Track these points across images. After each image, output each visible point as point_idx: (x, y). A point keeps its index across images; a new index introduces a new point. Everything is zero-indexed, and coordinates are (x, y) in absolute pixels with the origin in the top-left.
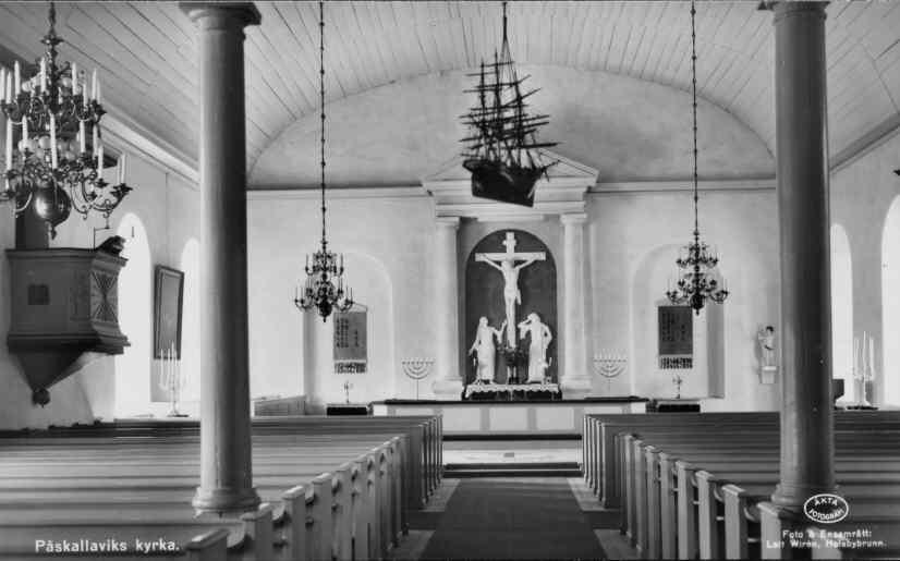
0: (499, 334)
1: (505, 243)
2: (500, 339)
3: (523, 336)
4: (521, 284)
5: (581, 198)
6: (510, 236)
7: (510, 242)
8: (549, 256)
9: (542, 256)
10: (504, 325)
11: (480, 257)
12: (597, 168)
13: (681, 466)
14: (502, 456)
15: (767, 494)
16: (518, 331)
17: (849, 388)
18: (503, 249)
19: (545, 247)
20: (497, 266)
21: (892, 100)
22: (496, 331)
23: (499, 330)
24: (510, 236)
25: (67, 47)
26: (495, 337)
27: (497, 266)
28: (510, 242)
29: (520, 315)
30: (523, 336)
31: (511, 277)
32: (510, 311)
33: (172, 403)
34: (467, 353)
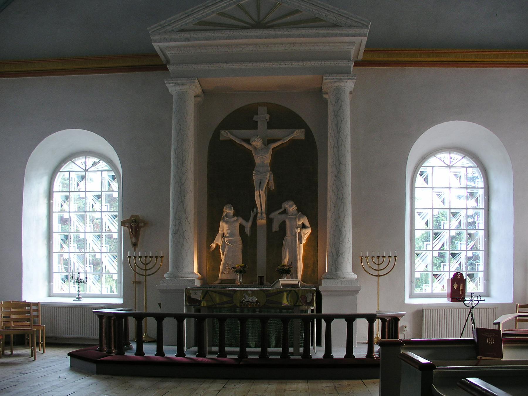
0: (248, 225)
1: (255, 118)
2: (248, 231)
3: (275, 227)
5: (296, 212)
7: (263, 117)
8: (308, 133)
9: (299, 134)
10: (252, 215)
11: (226, 135)
12: (236, 355)
13: (458, 383)
16: (270, 221)
18: (254, 126)
19: (215, 132)
20: (245, 145)
22: (244, 223)
26: (242, 228)
27: (245, 145)
28: (263, 117)
29: (274, 202)
30: (275, 227)
31: (263, 159)
32: (261, 199)
33: (86, 213)
34: (209, 247)
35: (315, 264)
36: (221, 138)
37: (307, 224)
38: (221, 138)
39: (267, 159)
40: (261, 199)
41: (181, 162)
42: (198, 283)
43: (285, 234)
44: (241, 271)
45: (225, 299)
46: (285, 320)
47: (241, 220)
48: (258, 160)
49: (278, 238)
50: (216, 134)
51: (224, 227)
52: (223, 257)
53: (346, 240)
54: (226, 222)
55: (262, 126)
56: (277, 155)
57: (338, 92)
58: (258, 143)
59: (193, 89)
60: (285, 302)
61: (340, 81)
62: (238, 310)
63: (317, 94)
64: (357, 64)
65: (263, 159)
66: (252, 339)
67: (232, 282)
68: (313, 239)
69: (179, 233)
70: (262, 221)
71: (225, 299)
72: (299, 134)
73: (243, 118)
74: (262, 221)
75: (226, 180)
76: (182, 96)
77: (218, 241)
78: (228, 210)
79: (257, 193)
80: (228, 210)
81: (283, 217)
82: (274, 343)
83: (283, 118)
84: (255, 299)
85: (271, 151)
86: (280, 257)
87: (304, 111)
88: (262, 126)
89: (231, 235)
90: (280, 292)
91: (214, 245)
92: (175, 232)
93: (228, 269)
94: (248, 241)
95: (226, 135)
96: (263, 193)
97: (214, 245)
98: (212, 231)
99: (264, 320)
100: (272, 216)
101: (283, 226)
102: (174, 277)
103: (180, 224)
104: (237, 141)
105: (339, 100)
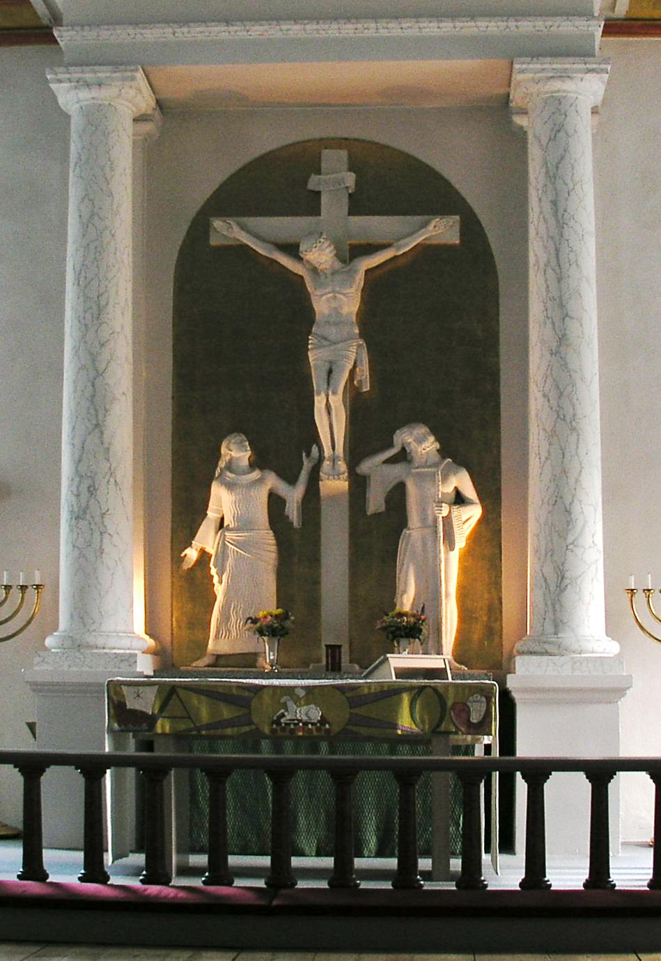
0: (294, 496)
2: (293, 512)
3: (375, 502)
4: (374, 321)
6: (334, 160)
7: (335, 180)
8: (471, 227)
9: (442, 230)
11: (227, 231)
14: (319, 398)
15: (589, 891)
16: (359, 484)
17: (131, 737)
18: (310, 204)
21: (39, 951)
22: (282, 488)
23: (292, 480)
24: (334, 160)
25: (99, 539)
26: (276, 503)
28: (335, 180)
30: (375, 502)
31: (338, 302)
32: (331, 419)
34: (178, 560)
35: (495, 609)
36: (214, 241)
37: (469, 491)
38: (214, 241)
39: (350, 302)
40: (331, 419)
41: (94, 311)
42: (145, 666)
43: (403, 523)
44: (272, 630)
45: (227, 712)
46: (407, 776)
47: (271, 481)
48: (321, 305)
49: (381, 533)
50: (199, 227)
51: (222, 501)
52: (219, 590)
53: (587, 540)
54: (230, 486)
55: (333, 206)
56: (379, 290)
57: (558, 107)
58: (321, 255)
59: (131, 98)
60: (406, 722)
61: (564, 76)
62: (265, 744)
63: (496, 113)
64: (613, 28)
65: (338, 302)
66: (307, 828)
67: (247, 662)
68: (489, 535)
69: (89, 516)
70: (335, 484)
71: (227, 712)
72: (442, 230)
73: (277, 183)
74: (335, 484)
75: (227, 362)
76: (96, 118)
77: (206, 539)
78: (236, 452)
79: (319, 402)
80: (236, 452)
81: (397, 471)
82: (372, 842)
83: (396, 183)
84: (315, 714)
85: (360, 279)
86: (390, 586)
87: (458, 161)
88: (333, 206)
89: (244, 524)
90: (390, 694)
91: (192, 554)
92: (79, 515)
93: (236, 622)
94: (295, 543)
95: (227, 231)
96: (337, 401)
97: (192, 554)
98: (188, 510)
99: (343, 776)
100: (365, 467)
101: (397, 496)
102: (76, 645)
103: (92, 490)
104: (261, 249)
105: (558, 131)
